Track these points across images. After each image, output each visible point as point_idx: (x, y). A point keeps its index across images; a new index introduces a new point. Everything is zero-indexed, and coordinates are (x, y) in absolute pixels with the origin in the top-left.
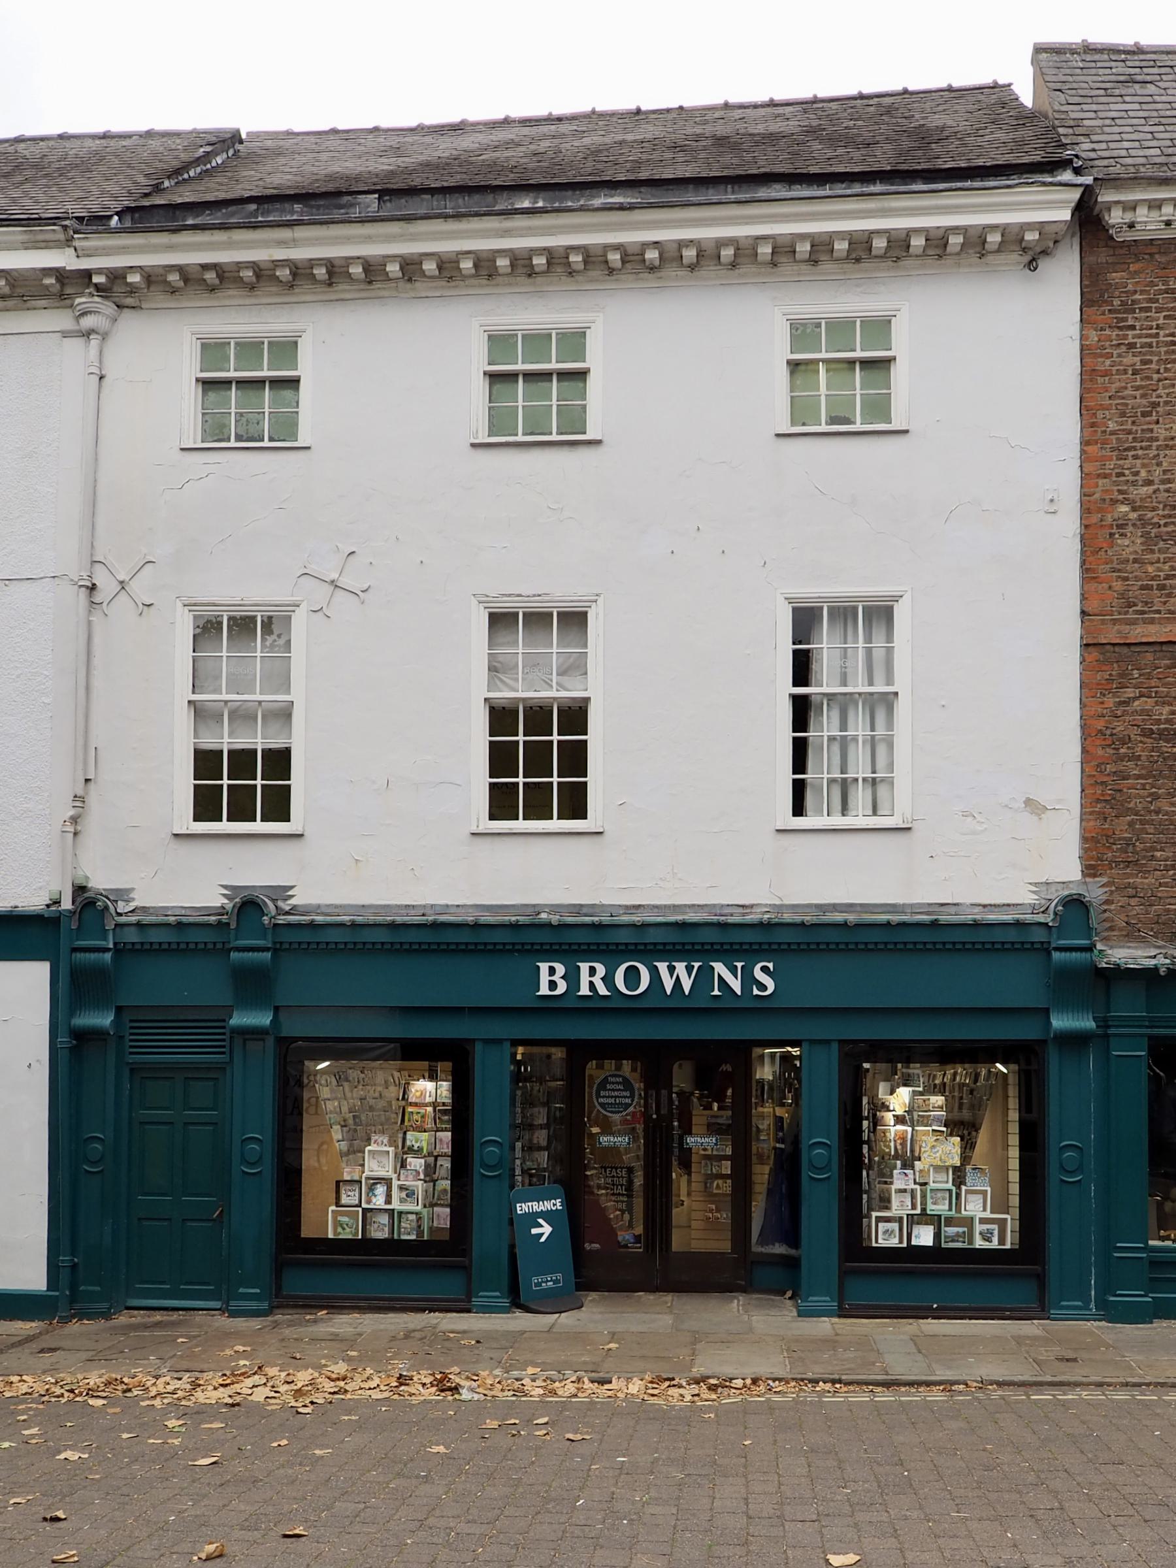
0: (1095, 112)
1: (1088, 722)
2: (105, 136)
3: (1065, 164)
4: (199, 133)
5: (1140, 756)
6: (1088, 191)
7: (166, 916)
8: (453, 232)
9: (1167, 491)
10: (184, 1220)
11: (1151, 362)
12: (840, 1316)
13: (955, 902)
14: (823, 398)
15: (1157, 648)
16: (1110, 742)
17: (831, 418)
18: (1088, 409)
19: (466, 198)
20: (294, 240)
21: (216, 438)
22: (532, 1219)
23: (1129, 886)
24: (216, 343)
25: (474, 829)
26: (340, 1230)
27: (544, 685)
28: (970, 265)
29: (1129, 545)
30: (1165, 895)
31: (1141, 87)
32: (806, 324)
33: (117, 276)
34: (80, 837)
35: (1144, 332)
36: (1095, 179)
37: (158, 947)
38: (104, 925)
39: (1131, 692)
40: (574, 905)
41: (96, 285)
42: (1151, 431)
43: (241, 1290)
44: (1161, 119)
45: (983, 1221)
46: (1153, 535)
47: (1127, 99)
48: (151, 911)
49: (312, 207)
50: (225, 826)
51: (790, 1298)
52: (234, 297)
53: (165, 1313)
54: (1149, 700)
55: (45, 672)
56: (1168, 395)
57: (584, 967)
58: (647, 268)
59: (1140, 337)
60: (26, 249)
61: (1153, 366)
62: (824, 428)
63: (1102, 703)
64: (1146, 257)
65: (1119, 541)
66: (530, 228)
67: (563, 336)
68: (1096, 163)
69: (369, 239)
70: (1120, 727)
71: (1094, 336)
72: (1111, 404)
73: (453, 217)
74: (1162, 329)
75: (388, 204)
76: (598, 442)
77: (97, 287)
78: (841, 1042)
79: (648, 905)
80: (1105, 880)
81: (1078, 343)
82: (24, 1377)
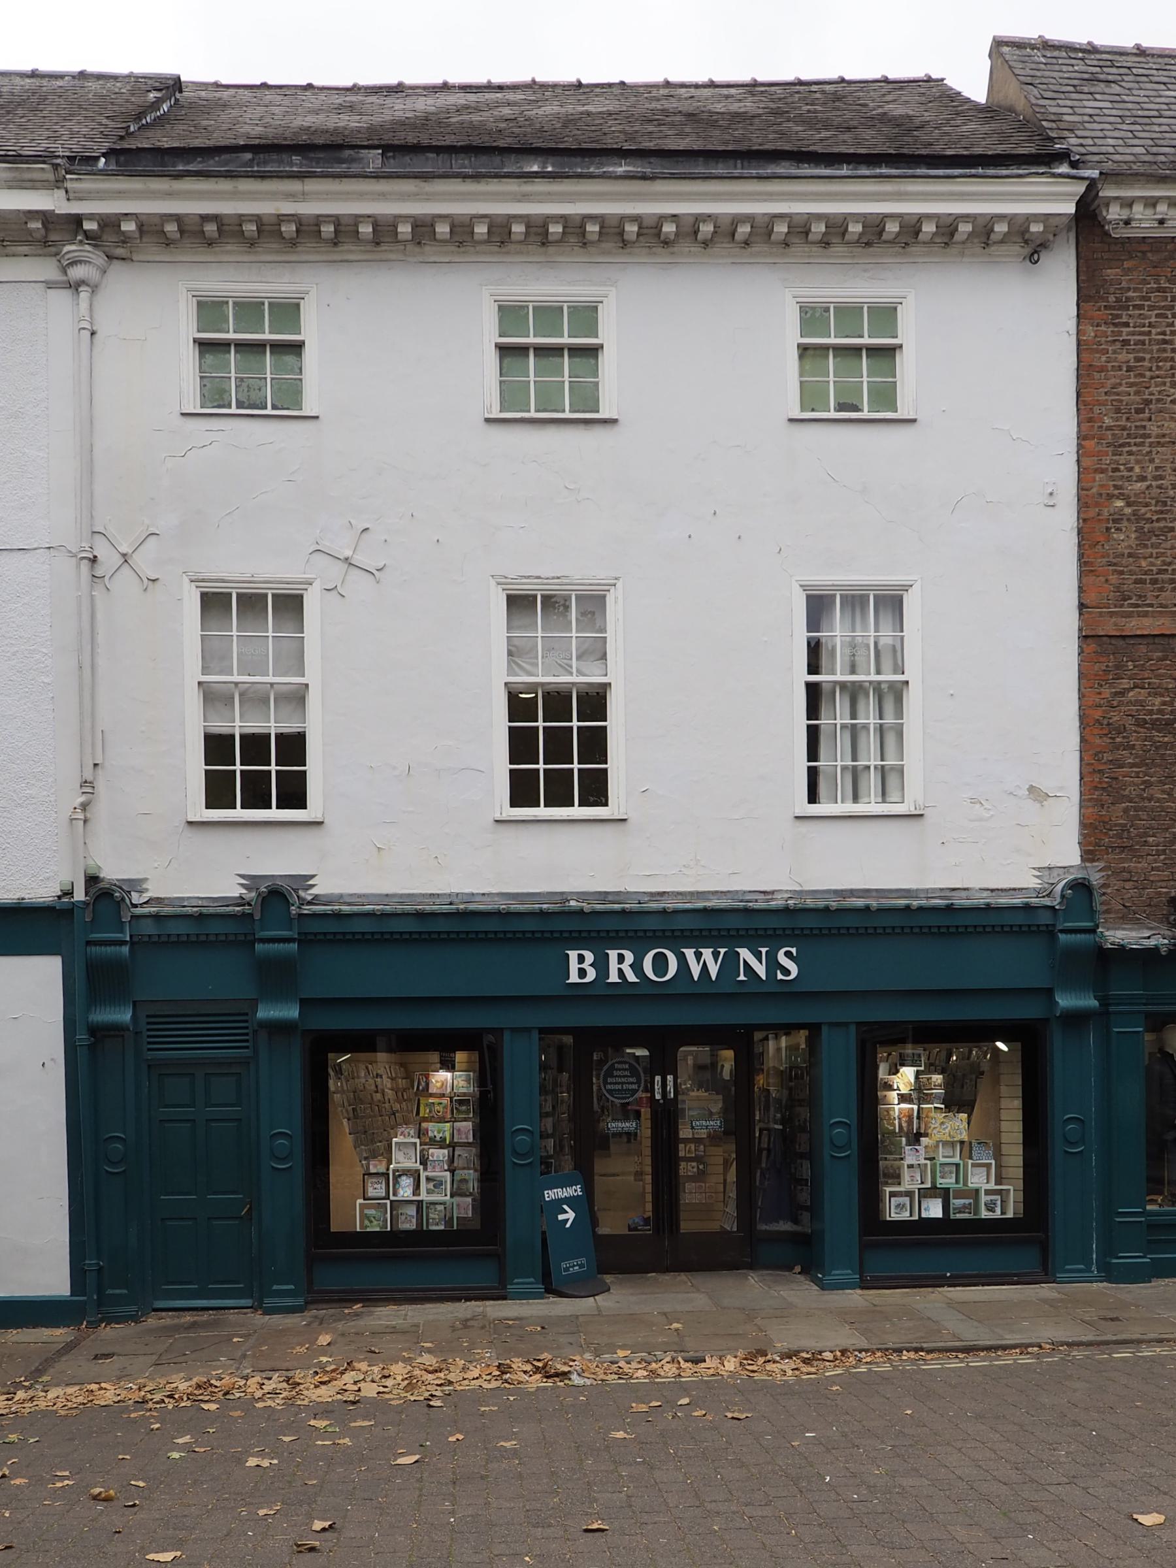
0: (1071, 107)
1: (1086, 712)
2: (34, 74)
3: (1063, 156)
4: (138, 77)
5: (1134, 745)
6: (1092, 185)
7: (184, 906)
8: (470, 193)
9: (1160, 487)
10: (209, 1218)
11: (1143, 359)
12: (862, 1288)
13: (965, 886)
14: (832, 384)
15: (1150, 640)
16: (1106, 732)
17: (839, 404)
18: (1086, 404)
19: (473, 159)
20: (303, 194)
21: (215, 404)
22: (557, 1206)
23: (1124, 870)
24: (213, 302)
25: (498, 817)
26: (367, 1222)
27: (561, 669)
28: (973, 255)
29: (1125, 539)
30: (1157, 878)
31: (1107, 86)
32: (815, 308)
33: (110, 223)
34: (89, 824)
35: (1137, 329)
36: (1101, 173)
37: (166, 939)
38: (120, 917)
39: (1126, 683)
40: (600, 893)
41: (85, 232)
42: (1144, 427)
43: (275, 1287)
44: (1137, 119)
45: (988, 1192)
46: (1146, 530)
47: (1098, 97)
48: (166, 902)
49: (311, 159)
50: (239, 813)
51: (799, 1273)
52: (228, 252)
53: (195, 1313)
54: (1142, 691)
55: (44, 650)
56: (1160, 392)
57: (613, 955)
58: (662, 242)
59: (1133, 334)
60: (10, 188)
61: (1146, 364)
62: (833, 414)
63: (1100, 693)
64: (1139, 254)
65: (1115, 535)
66: (549, 193)
67: (575, 310)
68: (1089, 158)
69: (383, 196)
70: (1115, 717)
71: (1090, 332)
72: (1107, 400)
73: (471, 177)
74: (1154, 327)
75: (392, 161)
76: (614, 421)
77: (88, 235)
78: (859, 1024)
79: (673, 892)
80: (1101, 865)
81: (1074, 338)
82: (103, 1385)
